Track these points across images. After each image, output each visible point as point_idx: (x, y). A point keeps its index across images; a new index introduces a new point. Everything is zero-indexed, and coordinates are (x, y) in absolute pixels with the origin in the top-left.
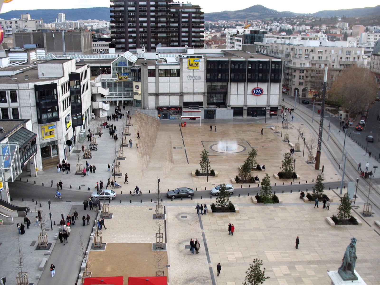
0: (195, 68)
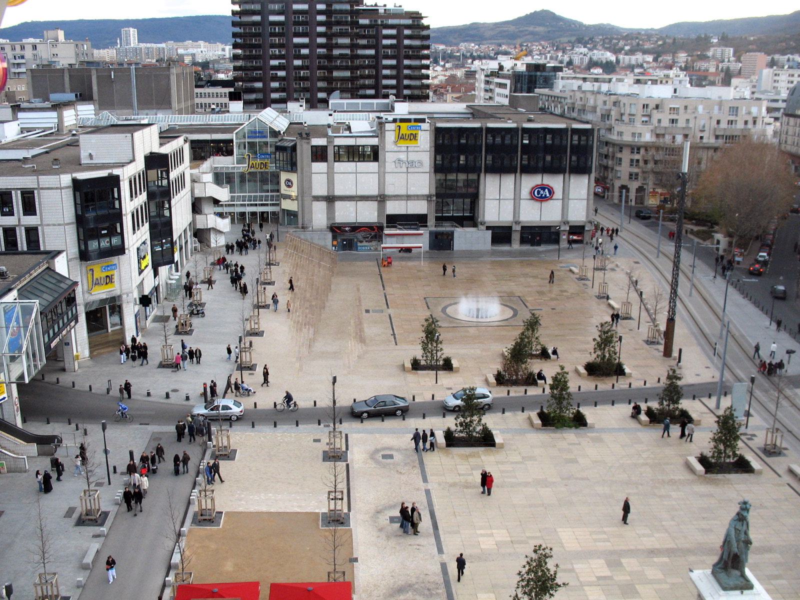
0: (411, 144)
